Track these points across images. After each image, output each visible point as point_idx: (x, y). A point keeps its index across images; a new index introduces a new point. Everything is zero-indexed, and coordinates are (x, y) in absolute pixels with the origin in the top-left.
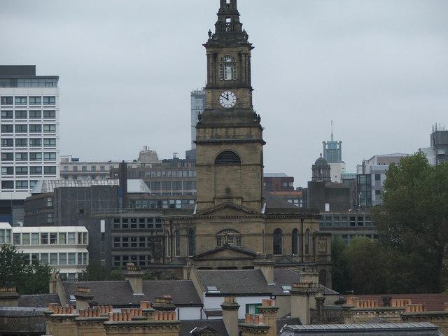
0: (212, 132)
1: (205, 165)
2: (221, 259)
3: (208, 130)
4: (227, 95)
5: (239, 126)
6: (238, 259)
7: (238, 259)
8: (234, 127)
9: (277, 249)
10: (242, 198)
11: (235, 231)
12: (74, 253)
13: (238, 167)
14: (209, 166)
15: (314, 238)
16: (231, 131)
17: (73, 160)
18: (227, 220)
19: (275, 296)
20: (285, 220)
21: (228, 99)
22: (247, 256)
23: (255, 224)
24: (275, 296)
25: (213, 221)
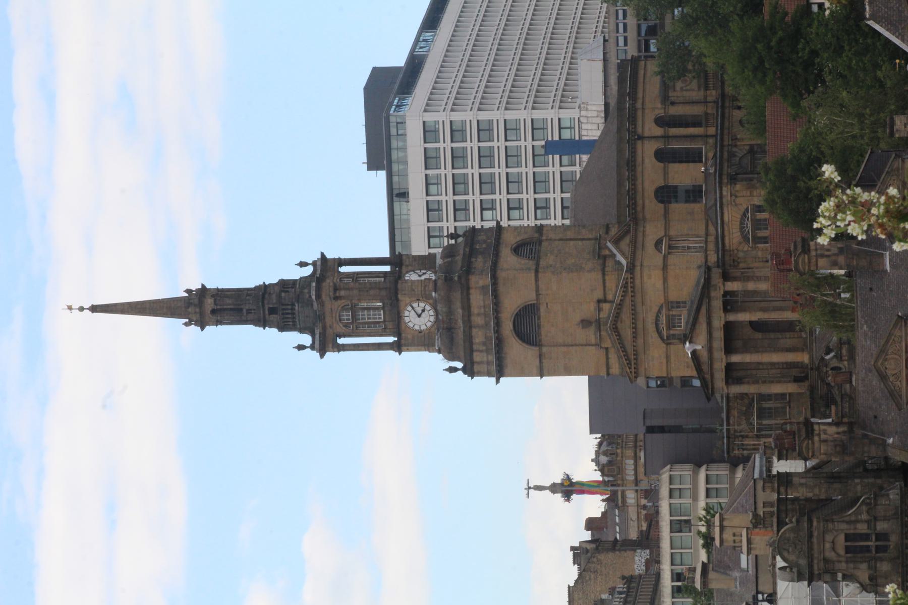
0: (481, 351)
1: (541, 362)
3: (477, 357)
4: (423, 311)
5: (467, 307)
9: (694, 194)
10: (599, 301)
11: (659, 311)
12: (707, 476)
14: (541, 356)
15: (673, 103)
16: (478, 320)
18: (640, 325)
19: (758, 592)
20: (639, 181)
21: (419, 316)
23: (645, 278)
24: (758, 592)
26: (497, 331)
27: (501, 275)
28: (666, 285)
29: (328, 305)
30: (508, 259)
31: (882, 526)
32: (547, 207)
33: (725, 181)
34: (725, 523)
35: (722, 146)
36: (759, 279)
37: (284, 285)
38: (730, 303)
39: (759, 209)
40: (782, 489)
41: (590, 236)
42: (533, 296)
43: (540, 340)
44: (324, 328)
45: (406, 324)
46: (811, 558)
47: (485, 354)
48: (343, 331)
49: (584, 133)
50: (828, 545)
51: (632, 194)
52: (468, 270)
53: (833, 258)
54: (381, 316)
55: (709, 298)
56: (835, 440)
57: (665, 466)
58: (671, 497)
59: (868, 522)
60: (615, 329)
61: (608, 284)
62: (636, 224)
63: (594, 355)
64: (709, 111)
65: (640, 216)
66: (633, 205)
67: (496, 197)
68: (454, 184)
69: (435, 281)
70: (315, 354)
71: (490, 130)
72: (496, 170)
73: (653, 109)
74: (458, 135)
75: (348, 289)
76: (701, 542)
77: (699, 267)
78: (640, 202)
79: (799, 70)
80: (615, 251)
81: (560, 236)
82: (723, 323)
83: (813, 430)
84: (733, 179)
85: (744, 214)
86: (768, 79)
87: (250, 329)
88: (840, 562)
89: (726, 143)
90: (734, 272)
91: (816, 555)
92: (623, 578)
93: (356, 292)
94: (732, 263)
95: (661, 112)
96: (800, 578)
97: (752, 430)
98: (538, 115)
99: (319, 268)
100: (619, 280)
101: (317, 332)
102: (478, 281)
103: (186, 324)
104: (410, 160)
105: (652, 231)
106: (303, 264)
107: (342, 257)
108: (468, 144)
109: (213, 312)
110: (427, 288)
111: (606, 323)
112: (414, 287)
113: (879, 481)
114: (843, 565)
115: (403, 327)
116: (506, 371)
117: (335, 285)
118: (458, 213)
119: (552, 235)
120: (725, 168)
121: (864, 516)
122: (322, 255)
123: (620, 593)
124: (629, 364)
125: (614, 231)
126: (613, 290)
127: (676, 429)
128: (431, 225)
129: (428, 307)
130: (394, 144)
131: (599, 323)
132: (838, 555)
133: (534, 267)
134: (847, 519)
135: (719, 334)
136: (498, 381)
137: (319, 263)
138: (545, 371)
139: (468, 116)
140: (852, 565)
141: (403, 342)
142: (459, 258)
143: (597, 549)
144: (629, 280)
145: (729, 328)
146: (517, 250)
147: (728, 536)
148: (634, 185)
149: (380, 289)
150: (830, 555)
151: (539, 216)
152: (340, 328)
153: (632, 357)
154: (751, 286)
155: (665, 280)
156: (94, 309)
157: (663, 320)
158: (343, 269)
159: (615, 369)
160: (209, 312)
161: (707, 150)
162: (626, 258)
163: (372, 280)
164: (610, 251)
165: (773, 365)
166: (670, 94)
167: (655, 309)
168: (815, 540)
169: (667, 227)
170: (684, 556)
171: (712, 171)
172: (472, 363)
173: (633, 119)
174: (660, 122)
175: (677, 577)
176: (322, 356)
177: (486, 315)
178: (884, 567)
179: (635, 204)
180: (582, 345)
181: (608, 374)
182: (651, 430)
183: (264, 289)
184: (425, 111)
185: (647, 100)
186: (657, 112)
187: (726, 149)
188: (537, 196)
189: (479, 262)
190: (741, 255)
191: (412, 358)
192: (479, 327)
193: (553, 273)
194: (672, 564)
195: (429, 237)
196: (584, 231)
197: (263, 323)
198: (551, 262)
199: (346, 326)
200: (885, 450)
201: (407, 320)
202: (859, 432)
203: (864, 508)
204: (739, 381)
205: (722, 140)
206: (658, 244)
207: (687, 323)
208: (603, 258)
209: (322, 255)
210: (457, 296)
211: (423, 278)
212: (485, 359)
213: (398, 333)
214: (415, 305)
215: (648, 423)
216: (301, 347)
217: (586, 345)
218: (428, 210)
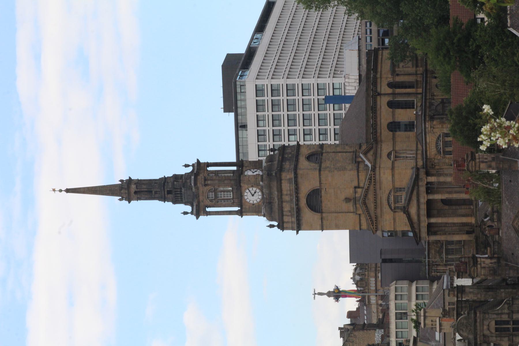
0: (288, 216)
2: (419, 215)
3: (286, 219)
4: (255, 192)
5: (280, 190)
8: (282, 195)
9: (410, 127)
10: (355, 188)
11: (390, 193)
13: (323, 192)
14: (322, 219)
15: (398, 75)
16: (286, 198)
18: (378, 201)
20: (378, 119)
21: (253, 195)
23: (382, 174)
25: (379, 215)
26: (297, 204)
27: (300, 172)
28: (394, 178)
30: (303, 163)
32: (326, 134)
33: (427, 119)
34: (427, 314)
35: (426, 99)
38: (430, 189)
40: (459, 295)
42: (319, 185)
43: (322, 210)
44: (199, 202)
47: (290, 217)
48: (209, 204)
49: (347, 91)
51: (375, 126)
52: (281, 169)
53: (489, 163)
54: (231, 195)
55: (418, 186)
58: (396, 299)
59: (508, 314)
60: (365, 203)
63: (352, 218)
64: (419, 79)
65: (379, 139)
66: (375, 133)
67: (297, 128)
68: (273, 120)
69: (262, 175)
70: (194, 217)
71: (294, 90)
73: (387, 78)
76: (413, 325)
77: (412, 168)
78: (379, 131)
80: (365, 159)
81: (333, 150)
82: (426, 200)
83: (477, 261)
84: (432, 118)
85: (438, 138)
87: (157, 202)
88: (492, 336)
89: (428, 98)
90: (433, 171)
94: (431, 166)
95: (391, 80)
97: (442, 261)
98: (321, 81)
100: (367, 175)
101: (195, 204)
102: (287, 176)
103: (120, 200)
105: (386, 148)
106: (187, 166)
107: (209, 162)
109: (136, 193)
110: (257, 180)
111: (359, 201)
112: (250, 179)
113: (515, 291)
114: (494, 338)
115: (243, 201)
116: (302, 227)
117: (205, 177)
118: (275, 137)
121: (506, 311)
122: (198, 160)
124: (372, 223)
125: (364, 147)
129: (258, 191)
130: (239, 97)
132: (491, 332)
133: (318, 168)
135: (424, 207)
136: (297, 233)
137: (196, 165)
138: (324, 227)
139: (281, 82)
140: (499, 339)
141: (243, 210)
142: (276, 163)
143: (354, 329)
144: (373, 176)
145: (429, 203)
149: (230, 180)
150: (486, 332)
151: (321, 139)
152: (208, 202)
154: (442, 179)
155: (393, 175)
156: (68, 191)
157: (392, 198)
158: (210, 169)
159: (364, 226)
160: (133, 193)
161: (417, 101)
162: (371, 163)
163: (226, 175)
164: (362, 158)
165: (454, 224)
166: (397, 69)
167: (387, 192)
168: (478, 324)
171: (420, 113)
173: (375, 84)
174: (391, 85)
176: (197, 218)
177: (291, 195)
179: (376, 132)
180: (346, 212)
181: (360, 229)
182: (384, 261)
183: (164, 180)
184: (257, 79)
185: (383, 73)
186: (389, 80)
187: (428, 101)
188: (320, 127)
189: (287, 165)
190: (436, 161)
191: (247, 218)
192: (287, 202)
193: (329, 171)
194: (397, 338)
195: (259, 150)
196: (347, 147)
198: (328, 165)
199: (211, 201)
201: (246, 197)
202: (503, 262)
203: (506, 306)
204: (435, 233)
205: (426, 96)
206: (389, 155)
207: (405, 200)
208: (358, 163)
209: (198, 160)
210: (274, 184)
212: (290, 220)
213: (241, 205)
214: (251, 189)
215: (383, 257)
216: (185, 213)
217: (348, 212)
218: (258, 135)
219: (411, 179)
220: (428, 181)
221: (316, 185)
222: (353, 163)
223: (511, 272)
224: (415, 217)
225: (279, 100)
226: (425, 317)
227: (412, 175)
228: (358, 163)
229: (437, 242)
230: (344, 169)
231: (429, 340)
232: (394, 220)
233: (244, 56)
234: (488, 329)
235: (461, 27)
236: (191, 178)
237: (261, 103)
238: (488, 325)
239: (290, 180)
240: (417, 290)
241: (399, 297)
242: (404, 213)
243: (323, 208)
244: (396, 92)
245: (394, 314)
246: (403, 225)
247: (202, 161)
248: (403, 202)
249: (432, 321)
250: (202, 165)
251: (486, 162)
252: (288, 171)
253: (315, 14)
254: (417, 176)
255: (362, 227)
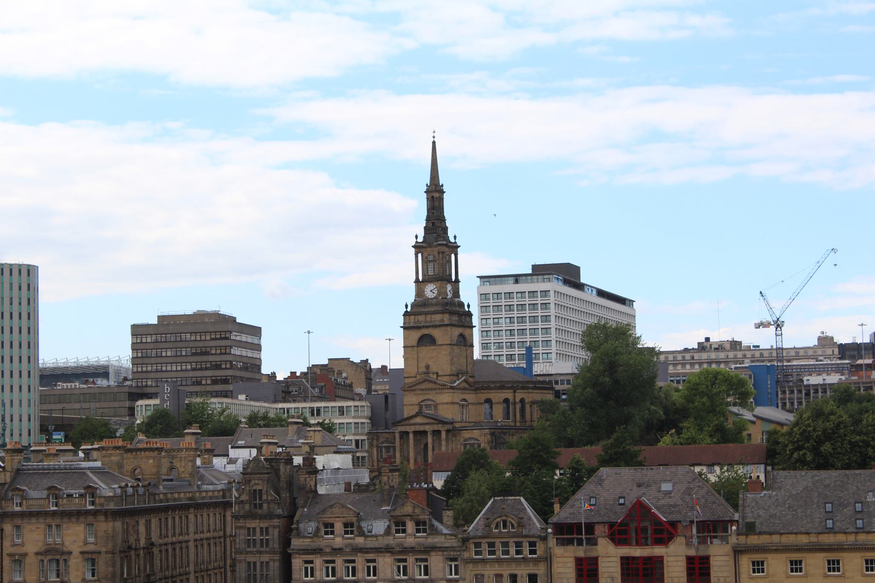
0: (415, 319)
1: (410, 347)
2: (411, 425)
3: (412, 317)
5: (435, 313)
6: (426, 424)
7: (426, 424)
10: (437, 373)
11: (433, 401)
13: (434, 347)
14: (413, 346)
15: (531, 406)
16: (429, 318)
17: (754, 346)
18: (427, 392)
20: (494, 391)
21: (431, 291)
22: (433, 421)
23: (448, 394)
24: (286, 448)
26: (424, 327)
27: (449, 328)
29: (436, 249)
30: (457, 331)
31: (265, 506)
32: (511, 347)
33: (492, 431)
34: (317, 432)
35: (509, 429)
36: (447, 446)
37: (445, 229)
38: (437, 433)
39: (479, 446)
40: (283, 461)
41: (468, 369)
42: (440, 343)
43: (422, 346)
44: (425, 247)
45: (427, 285)
46: (251, 474)
49: (536, 365)
50: (257, 481)
51: (488, 388)
52: (451, 313)
53: (388, 483)
54: (431, 273)
55: (438, 424)
56: (306, 484)
57: (370, 403)
58: (355, 406)
59: (267, 500)
60: (425, 381)
61: (446, 377)
62: (474, 390)
63: (413, 371)
64: (527, 423)
65: (478, 392)
66: (483, 388)
67: (516, 324)
68: (522, 305)
69: (446, 298)
70: (413, 244)
71: (546, 321)
72: (540, 323)
73: (528, 397)
74: (544, 306)
75: (443, 259)
76: (321, 421)
77: (453, 419)
78: (485, 391)
79: (528, 465)
80: (460, 380)
81: (468, 355)
82: (427, 430)
83: (312, 474)
84: (492, 434)
85: (476, 440)
86: (525, 451)
87: (426, 214)
88: (249, 487)
89: (511, 431)
90: (450, 435)
91: (252, 476)
92: (352, 383)
93: (441, 262)
95: (526, 401)
96: (244, 469)
97: (380, 444)
98: (553, 343)
99: (454, 245)
100: (447, 382)
101: (424, 244)
102: (446, 319)
103: (427, 184)
104: (532, 285)
105: (471, 397)
106: (455, 237)
108: (540, 311)
109: (433, 197)
111: (427, 376)
113: (288, 504)
114: (248, 489)
115: (426, 283)
116: (406, 331)
117: (444, 252)
118: (508, 307)
119: (469, 351)
120: (498, 431)
121: (270, 498)
122: (459, 246)
123: (344, 382)
124: (409, 387)
125: (471, 380)
126: (441, 380)
127: (387, 409)
128: (503, 294)
129: (435, 295)
130: (540, 277)
131: (428, 373)
132: (253, 486)
133: (453, 343)
134: (269, 490)
135: (422, 428)
136: (401, 327)
137: (455, 245)
138: (406, 349)
139: (552, 311)
140: (248, 492)
141: (419, 284)
142: (458, 309)
143: (367, 371)
145: (425, 433)
146: (462, 335)
147: (312, 433)
148: (492, 389)
149: (443, 273)
150: (253, 482)
151: (507, 344)
152: (425, 255)
153: (412, 388)
154: (444, 443)
155: (447, 403)
156: (434, 143)
157: (429, 403)
158: (453, 256)
159: (407, 381)
161: (510, 422)
162: (457, 385)
163: (448, 269)
164: (461, 378)
165: (409, 453)
166: (535, 405)
167: (434, 399)
168: (259, 476)
169: (473, 404)
170: (327, 413)
171: (499, 424)
172: (409, 315)
173: (523, 388)
174: (522, 401)
175: (318, 410)
176: (413, 247)
177: (431, 321)
178: (247, 507)
179: (484, 389)
181: (405, 378)
182: (386, 397)
183: (443, 220)
184: (555, 291)
185: (533, 394)
186: (527, 399)
187: (508, 431)
188: (516, 343)
189: (455, 318)
190: (458, 438)
191: (412, 287)
192: (426, 318)
193: (450, 352)
194: (324, 407)
195: (498, 294)
196: (471, 366)
197: (428, 219)
198: (455, 351)
199: (426, 258)
200: (301, 507)
201: (429, 285)
202: (311, 495)
203: (273, 498)
204: (401, 438)
205: (513, 429)
206: (465, 400)
207: (428, 414)
208: (457, 375)
209: (459, 246)
210: (440, 308)
211: (449, 293)
212: (411, 321)
213: (423, 282)
214: (436, 289)
215: (389, 396)
216: (417, 237)
217: (418, 367)
218: (510, 293)
219: (445, 418)
220: (442, 432)
221: (439, 342)
222: (458, 371)
223: (302, 502)
224: (413, 421)
225: (537, 309)
226: (315, 431)
227: (447, 419)
228: (457, 375)
229: (395, 439)
230: (452, 364)
231: (299, 434)
232: (412, 405)
233: (578, 282)
234: (255, 484)
235: (552, 458)
236: (444, 241)
237: (535, 295)
238: (258, 484)
239: (443, 320)
240: (363, 423)
241: (356, 409)
242: (417, 413)
243: (421, 348)
244: (517, 405)
245: (299, 406)
246: (408, 412)
247: (459, 249)
248: (426, 411)
249: (311, 437)
250: (456, 250)
251: (388, 481)
252: (450, 319)
253: (577, 341)
254: (446, 423)
255: (406, 379)
